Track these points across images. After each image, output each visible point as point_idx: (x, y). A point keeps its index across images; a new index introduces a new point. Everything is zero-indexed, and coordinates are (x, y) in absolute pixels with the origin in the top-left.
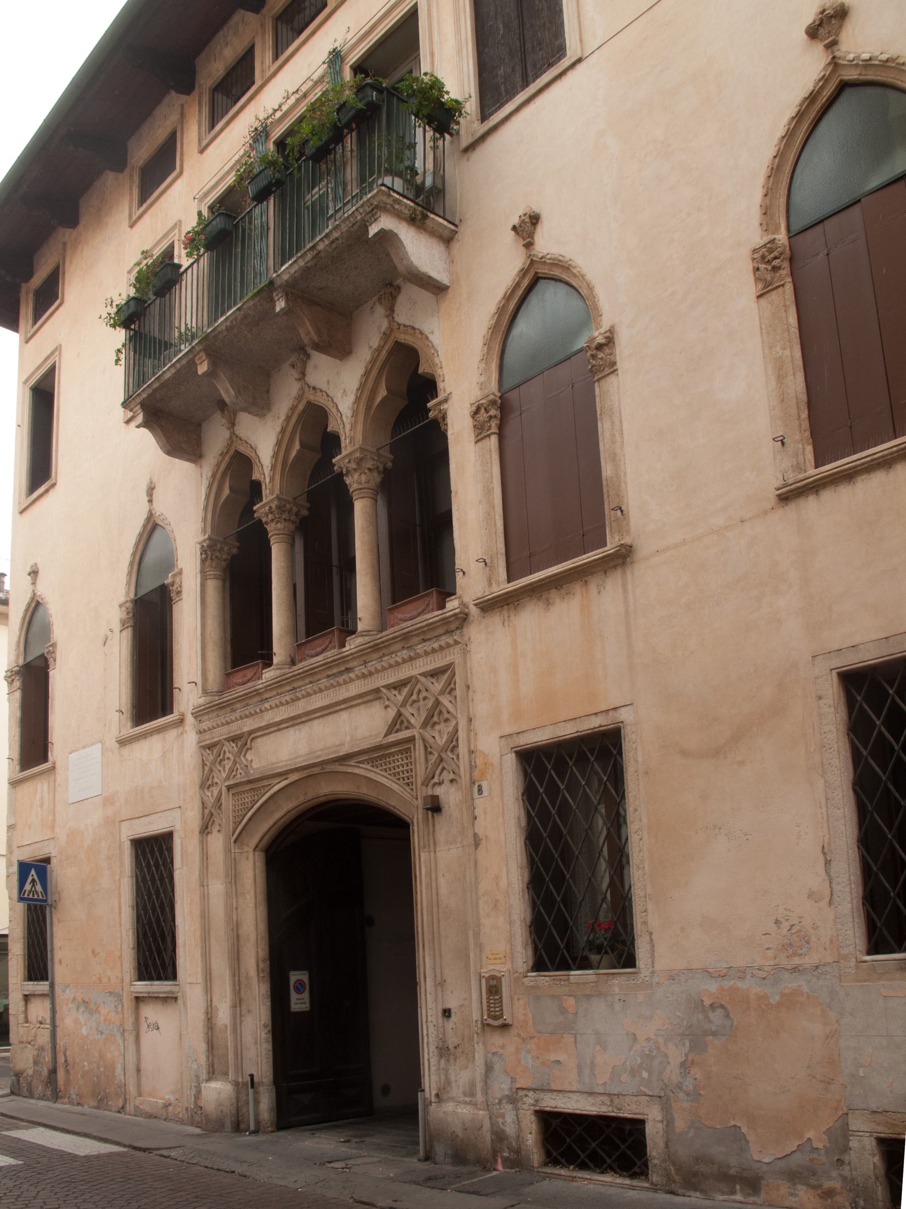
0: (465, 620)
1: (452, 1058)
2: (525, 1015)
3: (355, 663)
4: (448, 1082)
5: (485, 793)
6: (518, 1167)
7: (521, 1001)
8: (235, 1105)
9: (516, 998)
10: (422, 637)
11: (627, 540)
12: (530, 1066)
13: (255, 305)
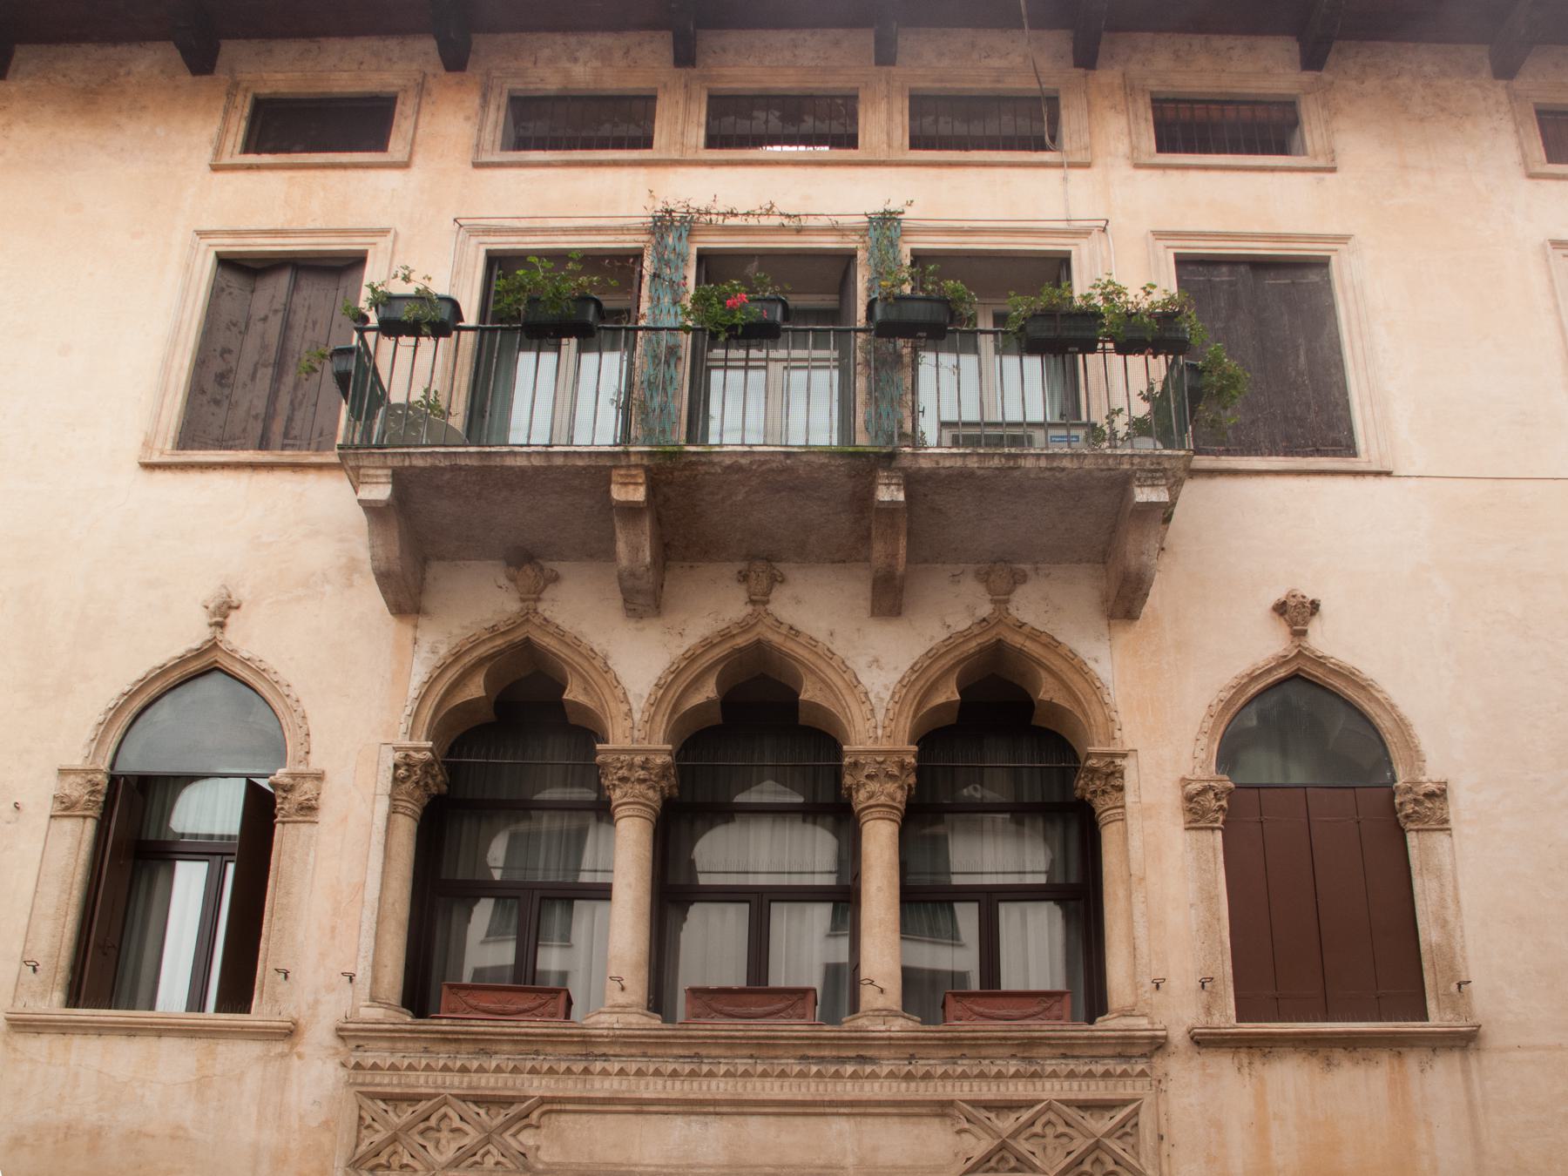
3: (885, 1053)
11: (1475, 1021)
13: (822, 466)
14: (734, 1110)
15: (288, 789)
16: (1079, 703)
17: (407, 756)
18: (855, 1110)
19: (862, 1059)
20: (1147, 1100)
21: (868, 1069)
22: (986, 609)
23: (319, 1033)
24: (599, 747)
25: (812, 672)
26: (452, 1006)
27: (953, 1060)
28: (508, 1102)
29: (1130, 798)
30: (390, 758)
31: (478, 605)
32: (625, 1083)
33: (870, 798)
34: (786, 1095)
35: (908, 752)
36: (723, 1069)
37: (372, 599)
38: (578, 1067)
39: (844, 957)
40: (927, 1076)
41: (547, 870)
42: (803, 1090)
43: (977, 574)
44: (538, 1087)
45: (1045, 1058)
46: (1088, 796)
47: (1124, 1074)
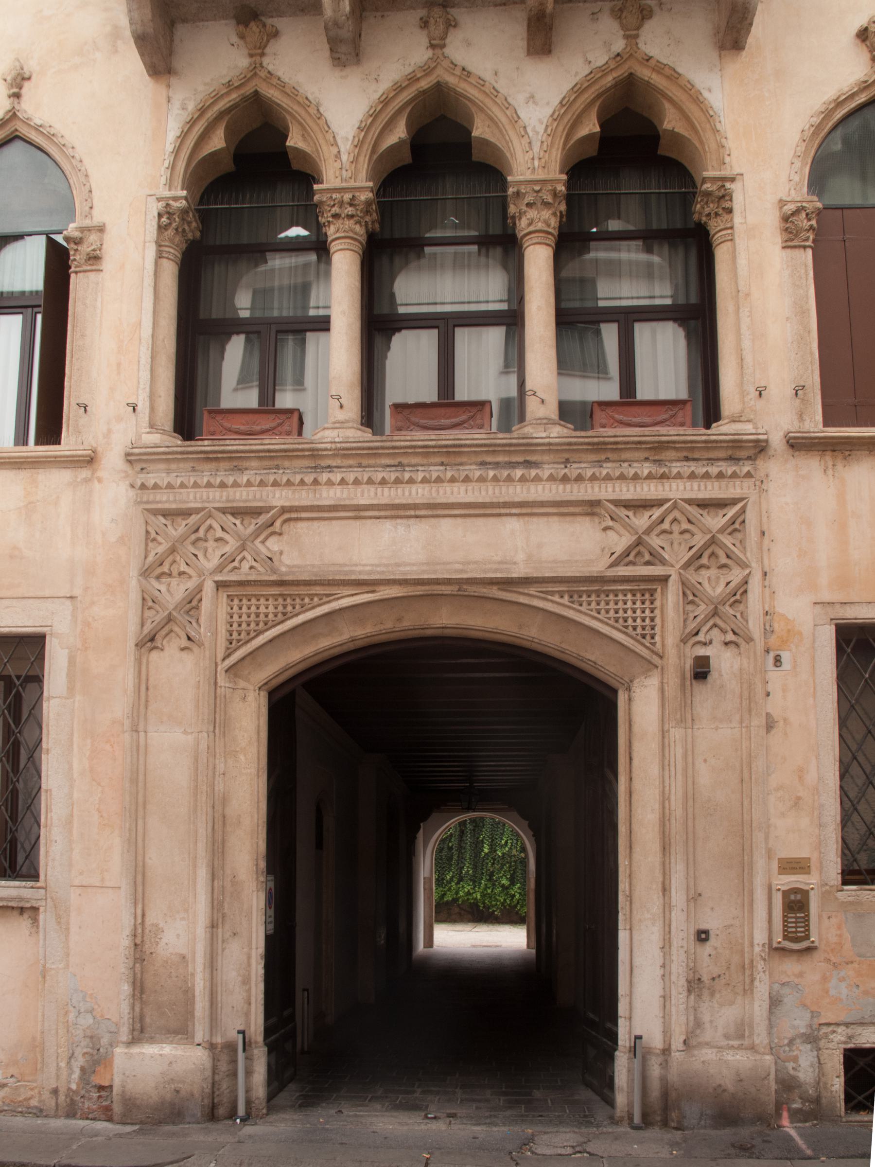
0: (761, 451)
1: (706, 993)
2: (840, 936)
3: (546, 458)
4: (698, 1024)
5: (786, 664)
6: (816, 1119)
7: (834, 920)
8: (210, 1080)
9: (825, 916)
10: (685, 454)
12: (844, 997)
14: (430, 513)
15: (78, 242)
16: (696, 132)
17: (168, 205)
18: (524, 511)
19: (528, 464)
20: (753, 498)
21: (533, 472)
22: (619, 45)
23: (113, 460)
24: (316, 187)
25: (482, 110)
26: (212, 429)
27: (599, 463)
28: (256, 512)
29: (737, 219)
30: (155, 207)
31: (217, 61)
32: (346, 491)
33: (530, 224)
34: (470, 498)
35: (558, 181)
36: (420, 476)
37: (132, 62)
38: (309, 479)
39: (514, 393)
40: (579, 478)
41: (281, 308)
42: (483, 493)
43: (612, 11)
44: (279, 498)
45: (671, 461)
46: (704, 219)
47: (734, 475)
